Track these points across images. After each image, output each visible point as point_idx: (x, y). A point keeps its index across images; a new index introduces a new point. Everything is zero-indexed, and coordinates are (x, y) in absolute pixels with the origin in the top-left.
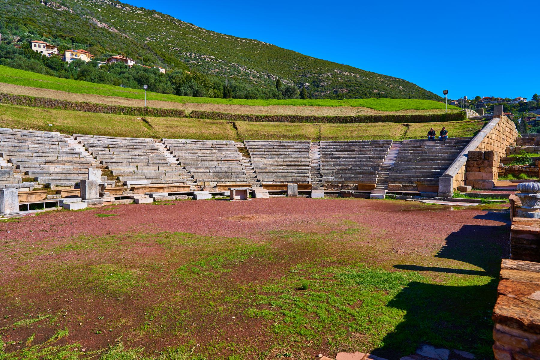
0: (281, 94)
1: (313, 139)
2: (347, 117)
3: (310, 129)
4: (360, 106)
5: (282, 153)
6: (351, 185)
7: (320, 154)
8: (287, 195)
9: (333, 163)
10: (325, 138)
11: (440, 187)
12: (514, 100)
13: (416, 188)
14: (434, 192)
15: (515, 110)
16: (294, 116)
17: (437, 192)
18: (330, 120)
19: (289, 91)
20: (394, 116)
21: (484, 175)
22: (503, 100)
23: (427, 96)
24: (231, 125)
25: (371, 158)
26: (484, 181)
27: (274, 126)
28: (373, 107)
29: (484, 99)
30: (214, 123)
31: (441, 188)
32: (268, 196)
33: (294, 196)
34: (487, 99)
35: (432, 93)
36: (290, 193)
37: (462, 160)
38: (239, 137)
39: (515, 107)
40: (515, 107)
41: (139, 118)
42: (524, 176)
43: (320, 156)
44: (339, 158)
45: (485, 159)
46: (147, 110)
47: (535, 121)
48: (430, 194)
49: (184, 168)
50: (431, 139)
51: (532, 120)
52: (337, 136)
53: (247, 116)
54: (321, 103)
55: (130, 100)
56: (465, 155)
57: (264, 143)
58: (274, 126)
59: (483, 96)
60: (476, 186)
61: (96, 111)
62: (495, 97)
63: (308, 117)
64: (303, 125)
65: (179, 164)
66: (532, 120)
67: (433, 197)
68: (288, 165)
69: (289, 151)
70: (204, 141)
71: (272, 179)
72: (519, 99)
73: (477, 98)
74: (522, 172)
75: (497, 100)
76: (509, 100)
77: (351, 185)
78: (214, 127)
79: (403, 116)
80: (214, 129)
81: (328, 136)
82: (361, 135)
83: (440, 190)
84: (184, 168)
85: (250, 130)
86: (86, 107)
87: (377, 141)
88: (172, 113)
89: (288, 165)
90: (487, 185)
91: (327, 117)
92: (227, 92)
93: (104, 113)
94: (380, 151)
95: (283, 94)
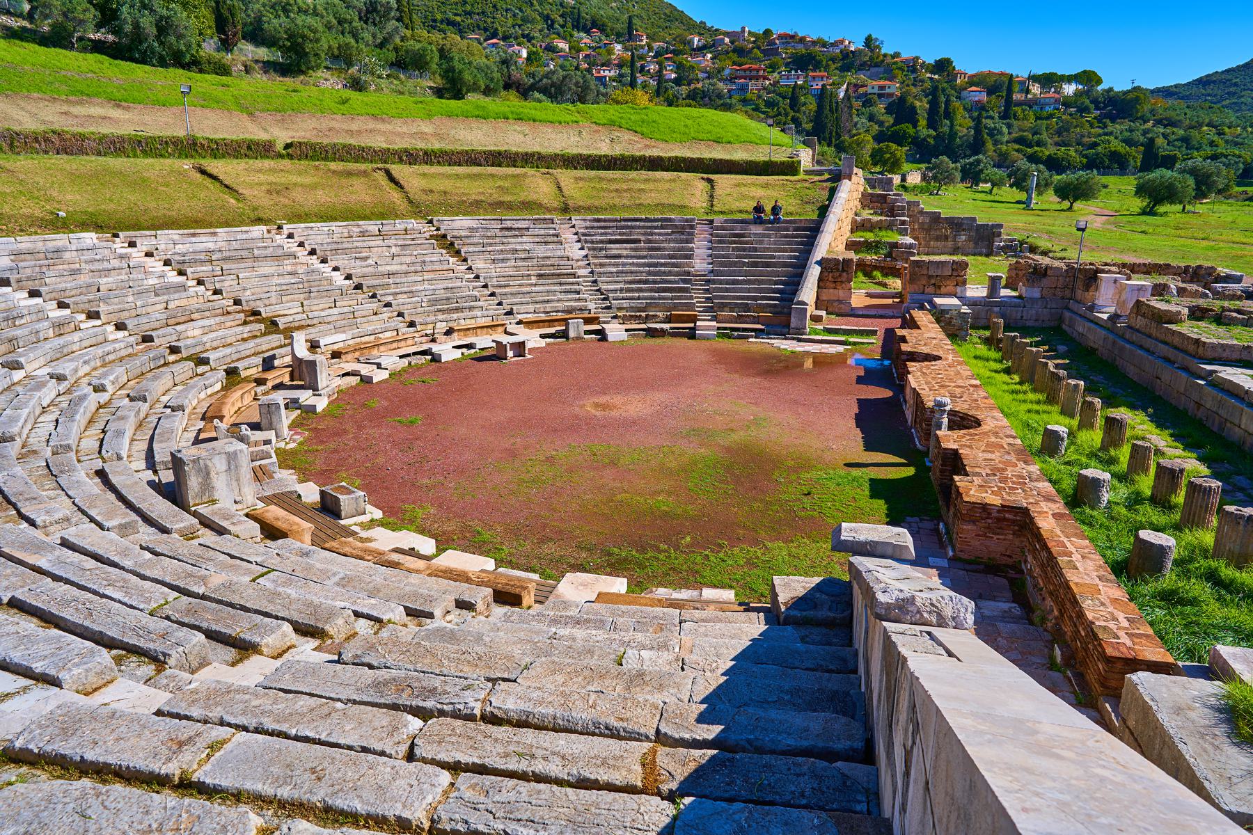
0: (357, 18)
1: (555, 209)
2: (600, 157)
3: (539, 186)
4: (611, 124)
5: (518, 247)
6: (660, 314)
7: (582, 248)
8: (567, 338)
9: (615, 270)
10: (579, 209)
11: (793, 320)
12: (832, 45)
13: (756, 320)
14: (784, 327)
15: (833, 66)
16: (499, 153)
17: (788, 325)
18: (571, 162)
19: (375, 10)
20: (684, 160)
21: (841, 293)
22: (814, 43)
23: (665, 14)
24: (382, 173)
25: (671, 257)
26: (840, 301)
27: (472, 177)
28: (638, 129)
29: (781, 37)
30: (349, 174)
31: (794, 322)
32: (543, 343)
33: (578, 338)
34: (789, 38)
35: (675, 9)
36: (572, 334)
37: (814, 272)
38: (417, 209)
39: (833, 60)
40: (833, 60)
41: (186, 165)
42: (877, 274)
43: (583, 253)
44: (619, 257)
45: (843, 270)
46: (195, 144)
47: (866, 94)
48: (779, 330)
49: (374, 296)
50: (758, 221)
51: (861, 90)
52: (597, 203)
53: (406, 151)
54: (538, 115)
55: (127, 109)
56: (817, 263)
57: (474, 224)
58: (472, 177)
59: (778, 29)
60: (830, 310)
61: (82, 151)
62: (801, 35)
63: (527, 154)
64: (525, 175)
65: (358, 287)
66: (861, 90)
67: (783, 335)
68: (540, 276)
69: (526, 242)
70: (361, 223)
71: (531, 308)
72: (842, 42)
73: (767, 32)
74: (876, 268)
75: (802, 40)
76: (824, 44)
77: (660, 314)
78: (358, 183)
79: (699, 159)
80: (359, 192)
81: (581, 203)
82: (638, 202)
83: (792, 325)
84: (374, 296)
85: (431, 191)
86: (57, 143)
87: (670, 220)
88: (249, 148)
89: (540, 276)
90: (844, 309)
91: (563, 156)
92: (226, 13)
93: (99, 154)
94: (681, 241)
95: (360, 19)
